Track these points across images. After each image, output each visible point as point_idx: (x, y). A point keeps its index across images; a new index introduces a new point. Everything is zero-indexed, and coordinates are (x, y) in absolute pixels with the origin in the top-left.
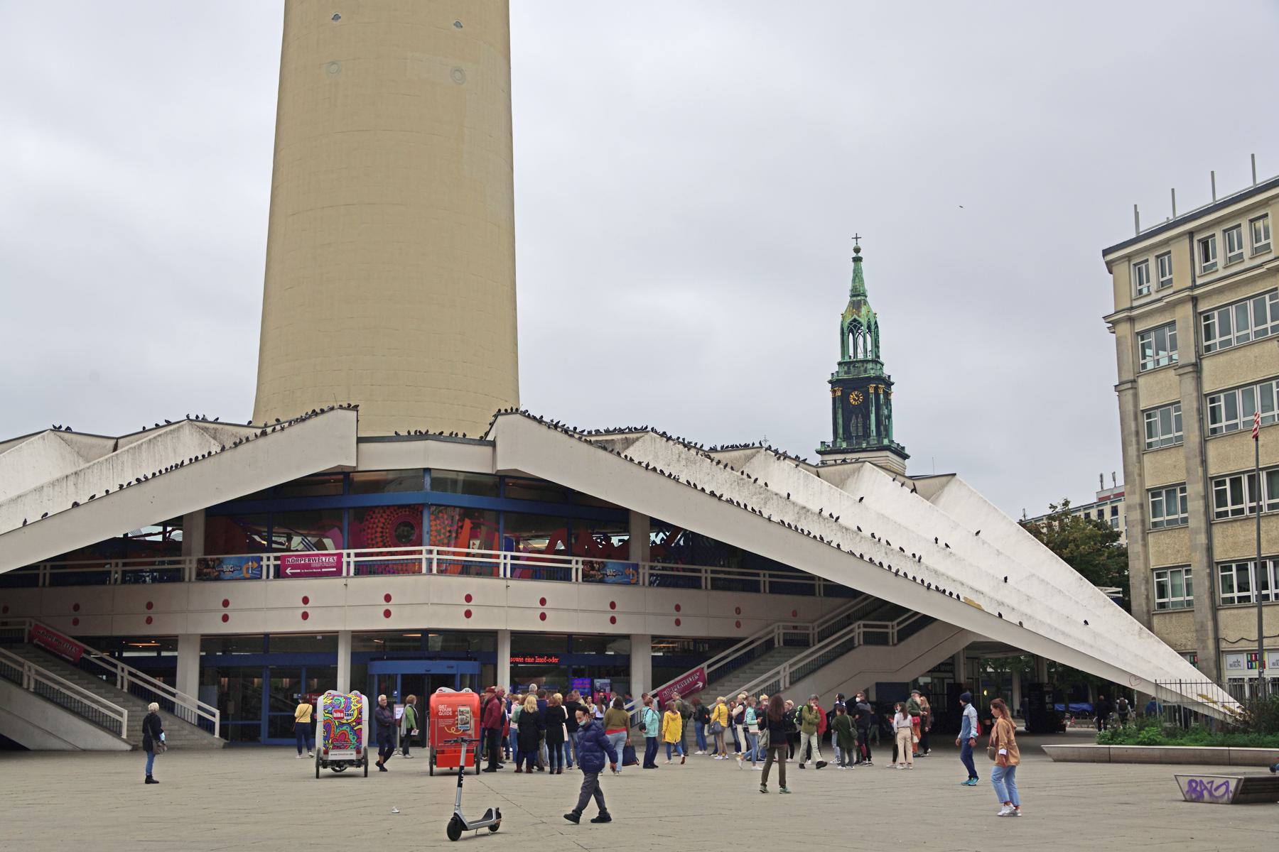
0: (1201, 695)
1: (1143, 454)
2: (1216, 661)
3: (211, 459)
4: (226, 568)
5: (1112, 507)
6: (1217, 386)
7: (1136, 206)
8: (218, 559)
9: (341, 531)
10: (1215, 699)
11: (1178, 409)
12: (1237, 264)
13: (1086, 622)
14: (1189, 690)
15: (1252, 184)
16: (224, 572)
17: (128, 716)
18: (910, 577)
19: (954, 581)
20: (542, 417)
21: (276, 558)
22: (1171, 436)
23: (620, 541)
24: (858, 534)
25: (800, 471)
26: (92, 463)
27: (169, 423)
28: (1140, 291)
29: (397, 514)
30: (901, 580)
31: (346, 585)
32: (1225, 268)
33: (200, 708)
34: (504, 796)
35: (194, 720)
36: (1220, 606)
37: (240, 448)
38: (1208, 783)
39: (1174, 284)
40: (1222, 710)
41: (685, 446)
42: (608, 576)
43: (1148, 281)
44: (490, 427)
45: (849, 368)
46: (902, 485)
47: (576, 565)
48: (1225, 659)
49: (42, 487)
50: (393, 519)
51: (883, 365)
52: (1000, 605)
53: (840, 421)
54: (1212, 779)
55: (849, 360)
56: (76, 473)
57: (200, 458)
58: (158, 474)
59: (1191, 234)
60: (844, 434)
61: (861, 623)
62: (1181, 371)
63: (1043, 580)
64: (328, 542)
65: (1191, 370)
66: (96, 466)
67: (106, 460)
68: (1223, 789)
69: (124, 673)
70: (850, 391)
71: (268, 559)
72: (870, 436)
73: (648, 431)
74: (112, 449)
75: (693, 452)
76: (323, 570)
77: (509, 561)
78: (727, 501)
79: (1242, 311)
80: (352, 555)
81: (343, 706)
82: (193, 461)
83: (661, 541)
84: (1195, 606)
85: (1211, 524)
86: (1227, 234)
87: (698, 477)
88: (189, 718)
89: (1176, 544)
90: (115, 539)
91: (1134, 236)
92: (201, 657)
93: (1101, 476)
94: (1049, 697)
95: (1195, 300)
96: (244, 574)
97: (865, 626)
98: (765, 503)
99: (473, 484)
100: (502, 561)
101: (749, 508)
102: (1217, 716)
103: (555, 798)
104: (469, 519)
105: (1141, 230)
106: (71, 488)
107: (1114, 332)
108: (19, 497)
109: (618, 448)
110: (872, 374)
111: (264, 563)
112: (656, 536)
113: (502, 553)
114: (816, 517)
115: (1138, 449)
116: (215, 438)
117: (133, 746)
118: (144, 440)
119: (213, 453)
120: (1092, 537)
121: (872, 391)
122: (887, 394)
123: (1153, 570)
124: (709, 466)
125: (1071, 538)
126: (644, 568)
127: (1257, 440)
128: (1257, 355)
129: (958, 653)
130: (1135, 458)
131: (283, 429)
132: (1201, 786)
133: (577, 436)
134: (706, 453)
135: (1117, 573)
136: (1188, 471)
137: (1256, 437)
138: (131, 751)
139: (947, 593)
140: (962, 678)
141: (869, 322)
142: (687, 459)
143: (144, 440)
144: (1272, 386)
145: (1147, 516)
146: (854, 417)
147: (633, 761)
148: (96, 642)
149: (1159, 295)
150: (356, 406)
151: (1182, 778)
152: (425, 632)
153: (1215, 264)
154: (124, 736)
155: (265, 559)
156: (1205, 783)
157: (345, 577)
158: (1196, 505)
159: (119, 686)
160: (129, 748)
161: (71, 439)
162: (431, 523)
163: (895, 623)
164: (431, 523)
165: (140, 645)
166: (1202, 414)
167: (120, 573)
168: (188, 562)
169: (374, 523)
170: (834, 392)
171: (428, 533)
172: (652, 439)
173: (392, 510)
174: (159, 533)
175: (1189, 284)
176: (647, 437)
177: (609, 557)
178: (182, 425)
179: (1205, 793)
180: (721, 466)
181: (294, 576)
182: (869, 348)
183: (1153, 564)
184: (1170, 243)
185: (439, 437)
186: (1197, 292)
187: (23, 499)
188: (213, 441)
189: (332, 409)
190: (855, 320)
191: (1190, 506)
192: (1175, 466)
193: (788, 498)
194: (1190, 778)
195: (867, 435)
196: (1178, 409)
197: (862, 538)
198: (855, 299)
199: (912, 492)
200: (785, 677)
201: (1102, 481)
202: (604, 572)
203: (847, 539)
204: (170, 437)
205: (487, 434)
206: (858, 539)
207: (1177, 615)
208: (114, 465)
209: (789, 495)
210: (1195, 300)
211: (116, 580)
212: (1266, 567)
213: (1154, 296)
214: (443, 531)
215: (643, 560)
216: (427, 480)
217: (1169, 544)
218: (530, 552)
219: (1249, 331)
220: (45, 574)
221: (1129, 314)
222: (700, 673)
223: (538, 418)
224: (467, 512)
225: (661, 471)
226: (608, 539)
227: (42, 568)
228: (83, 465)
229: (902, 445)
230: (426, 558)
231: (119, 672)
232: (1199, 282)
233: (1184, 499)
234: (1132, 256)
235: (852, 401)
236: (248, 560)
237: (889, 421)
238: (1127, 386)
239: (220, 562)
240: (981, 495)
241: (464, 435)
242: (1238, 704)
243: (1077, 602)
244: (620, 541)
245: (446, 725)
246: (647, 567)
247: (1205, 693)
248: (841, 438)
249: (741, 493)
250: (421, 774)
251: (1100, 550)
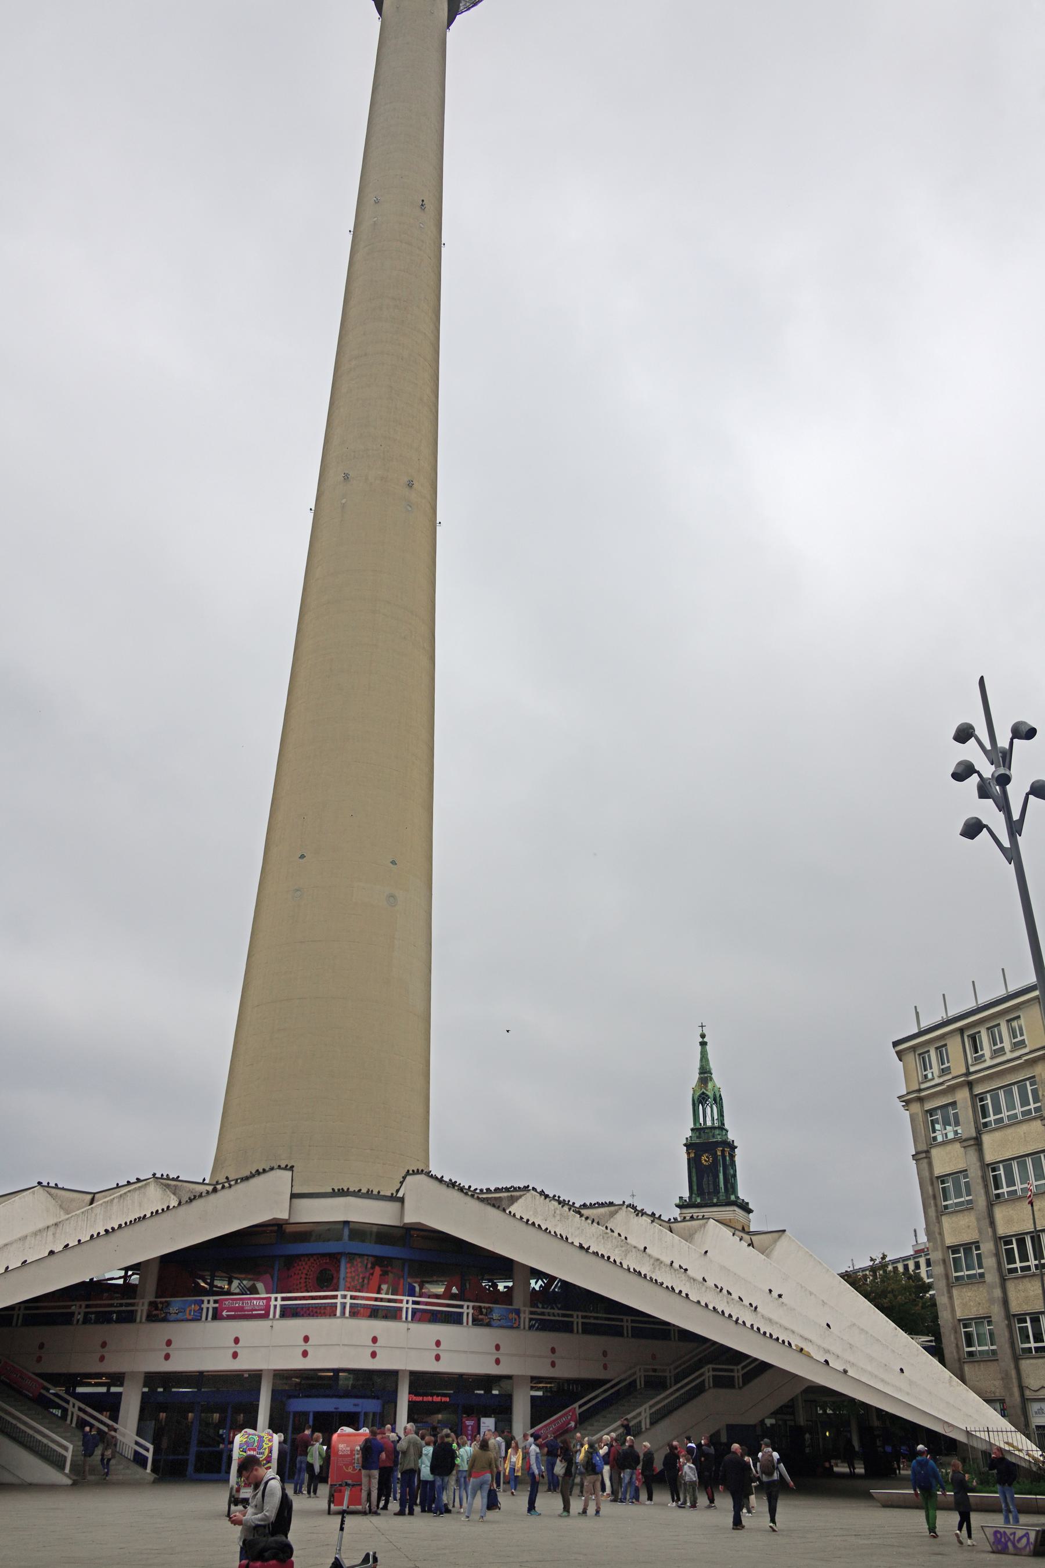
0: (1007, 1443)
1: (941, 1215)
2: (1023, 1408)
3: (169, 1212)
4: (173, 1310)
5: (926, 1259)
6: (996, 1158)
7: (916, 1007)
8: (166, 1302)
9: (272, 1278)
10: (1020, 1447)
11: (966, 1177)
12: (1022, 1048)
13: (902, 1370)
14: (996, 1438)
15: (975, 1005)
16: (170, 1314)
17: (73, 1451)
18: (748, 1325)
19: (786, 1329)
20: (442, 1177)
21: (215, 1302)
22: (962, 1199)
23: (505, 1287)
24: (703, 1285)
25: (655, 1226)
26: (70, 1215)
27: (138, 1180)
28: (926, 1076)
29: (319, 1262)
30: (741, 1328)
31: (272, 1327)
32: (992, 1058)
33: (137, 1443)
34: (388, 1537)
35: (131, 1456)
36: (1020, 1355)
37: (194, 1203)
38: (1011, 1534)
39: (952, 1071)
40: (1027, 1457)
41: (560, 1203)
42: (494, 1320)
43: (931, 1068)
44: (400, 1185)
45: (700, 1134)
46: (741, 1240)
47: (467, 1309)
48: (1030, 1407)
49: (26, 1236)
50: (316, 1266)
51: (727, 1131)
52: (826, 1352)
53: (694, 1179)
54: (1014, 1530)
55: (699, 1127)
56: (56, 1224)
57: (160, 1211)
58: (123, 1225)
59: (961, 1031)
60: (698, 1190)
61: (710, 1366)
62: (966, 1144)
63: (862, 1330)
64: (260, 1286)
65: (973, 1143)
66: (73, 1218)
67: (83, 1213)
68: (1024, 1540)
69: (74, 1408)
70: (701, 1153)
71: (209, 1302)
72: (719, 1192)
73: (530, 1190)
74: (89, 1202)
75: (566, 1208)
76: (254, 1312)
77: (410, 1306)
78: (594, 1253)
79: (1009, 1094)
80: (279, 1299)
81: (256, 1444)
82: (154, 1214)
83: (540, 1288)
84: (999, 1356)
85: (1005, 1280)
86: (938, 1051)
87: (570, 1230)
88: (126, 1453)
89: (976, 1296)
90: (84, 1283)
91: (916, 1031)
92: (143, 1393)
93: (915, 1231)
94: (880, 1441)
95: (970, 1085)
96: (187, 1316)
97: (714, 1370)
98: (626, 1255)
99: (384, 1235)
100: (404, 1305)
101: (612, 1260)
102: (1023, 1464)
103: (432, 1540)
104: (380, 1266)
105: (922, 1026)
106: (50, 1238)
107: (907, 1110)
108: (6, 1245)
109: (504, 1204)
110: (719, 1138)
111: (205, 1306)
112: (536, 1283)
113: (405, 1298)
114: (668, 1268)
115: (937, 1211)
116: (174, 1194)
117: (74, 1480)
118: (115, 1195)
119: (171, 1207)
120: (905, 1288)
121: (719, 1153)
122: (732, 1157)
123: (960, 1320)
124: (579, 1221)
125: (889, 1289)
126: (524, 1313)
127: (1032, 1206)
128: (1025, 1131)
129: (797, 1396)
130: (934, 1218)
131: (230, 1186)
132: (1005, 1538)
133: (470, 1193)
134: (577, 1210)
135: (931, 1322)
136: (980, 1232)
137: (1031, 1203)
138: (71, 1485)
139: (780, 1341)
140: (802, 1421)
141: (715, 1095)
142: (561, 1214)
143: (115, 1195)
144: (1041, 1158)
145: (949, 1271)
146: (706, 1176)
147: (494, 1506)
148: (55, 1379)
149: (941, 1080)
150: (292, 1167)
151: (987, 1528)
152: (336, 1371)
153: (983, 1055)
154: (67, 1471)
155: (206, 1302)
156: (1008, 1534)
157: (272, 1320)
158: (990, 1262)
159: (68, 1421)
160: (69, 1482)
161: (57, 1194)
162: (347, 1271)
163: (740, 1367)
164: (347, 1271)
165: (93, 1381)
166: (986, 1181)
167: (82, 1314)
168: (141, 1304)
169: (300, 1270)
170: (688, 1153)
171: (344, 1279)
172: (532, 1197)
173: (316, 1259)
174: (120, 1278)
175: (964, 1071)
176: (528, 1195)
177: (496, 1302)
178: (149, 1183)
179: (1010, 1544)
180: (589, 1221)
181: (229, 1318)
182: (716, 1117)
183: (959, 1315)
184: (945, 1037)
185: (357, 1194)
187: (9, 1247)
188: (172, 1196)
189: (272, 1169)
190: (703, 1093)
191: (985, 1262)
192: (969, 1227)
193: (645, 1251)
194: (995, 1529)
195: (717, 1191)
196: (966, 1177)
197: (707, 1288)
198: (702, 1076)
199: (749, 1245)
200: (645, 1418)
201: (916, 1236)
202: (492, 1317)
203: (694, 1288)
204: (137, 1192)
205: (398, 1191)
206: (704, 1289)
207: (984, 1363)
208: (89, 1217)
209: (645, 1248)
210: (970, 1085)
211: (78, 1320)
212: (1040, 1321)
213: (937, 1081)
214: (356, 1278)
216: (346, 1232)
217: (970, 1296)
218: (429, 1298)
219: (1016, 1111)
220: (18, 1315)
221: (918, 1095)
222: (573, 1414)
223: (439, 1177)
224: (379, 1261)
225: (539, 1225)
226: (495, 1286)
227: (17, 1309)
228: (64, 1217)
229: (746, 1201)
230: (341, 1303)
231: (70, 1408)
232: (972, 1069)
233: (979, 1256)
234: (918, 1047)
235: (703, 1161)
237: (735, 1180)
238: (922, 1156)
239: (168, 1304)
240: (807, 1250)
241: (379, 1192)
242: (1040, 1453)
243: (893, 1351)
244: (505, 1287)
245: (344, 1465)
246: (527, 1312)
247: (1010, 1441)
248: (695, 1194)
249: (606, 1246)
250: (318, 1513)
251: (915, 1300)
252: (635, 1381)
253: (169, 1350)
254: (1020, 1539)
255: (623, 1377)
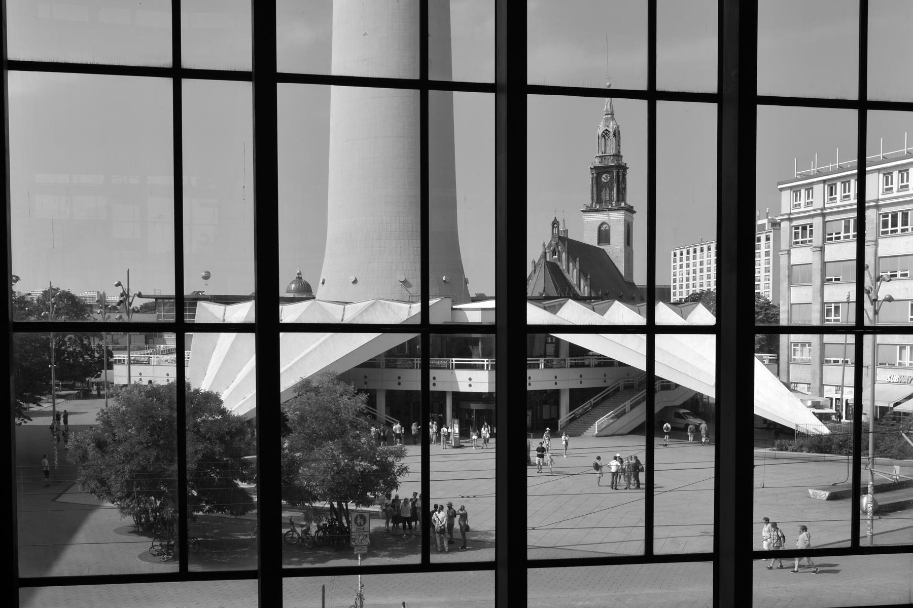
33: (386, 417)
35: (385, 423)
45: (602, 160)
53: (595, 192)
59: (824, 181)
62: (814, 249)
95: (824, 215)
96: (406, 366)
122: (624, 175)
153: (835, 199)
175: (821, 206)
179: (818, 496)
186: (825, 211)
190: (606, 130)
195: (611, 200)
215: (566, 357)
232: (827, 206)
235: (603, 180)
236: (408, 360)
252: (619, 387)
253: (400, 381)
254: (822, 495)
255: (614, 385)
